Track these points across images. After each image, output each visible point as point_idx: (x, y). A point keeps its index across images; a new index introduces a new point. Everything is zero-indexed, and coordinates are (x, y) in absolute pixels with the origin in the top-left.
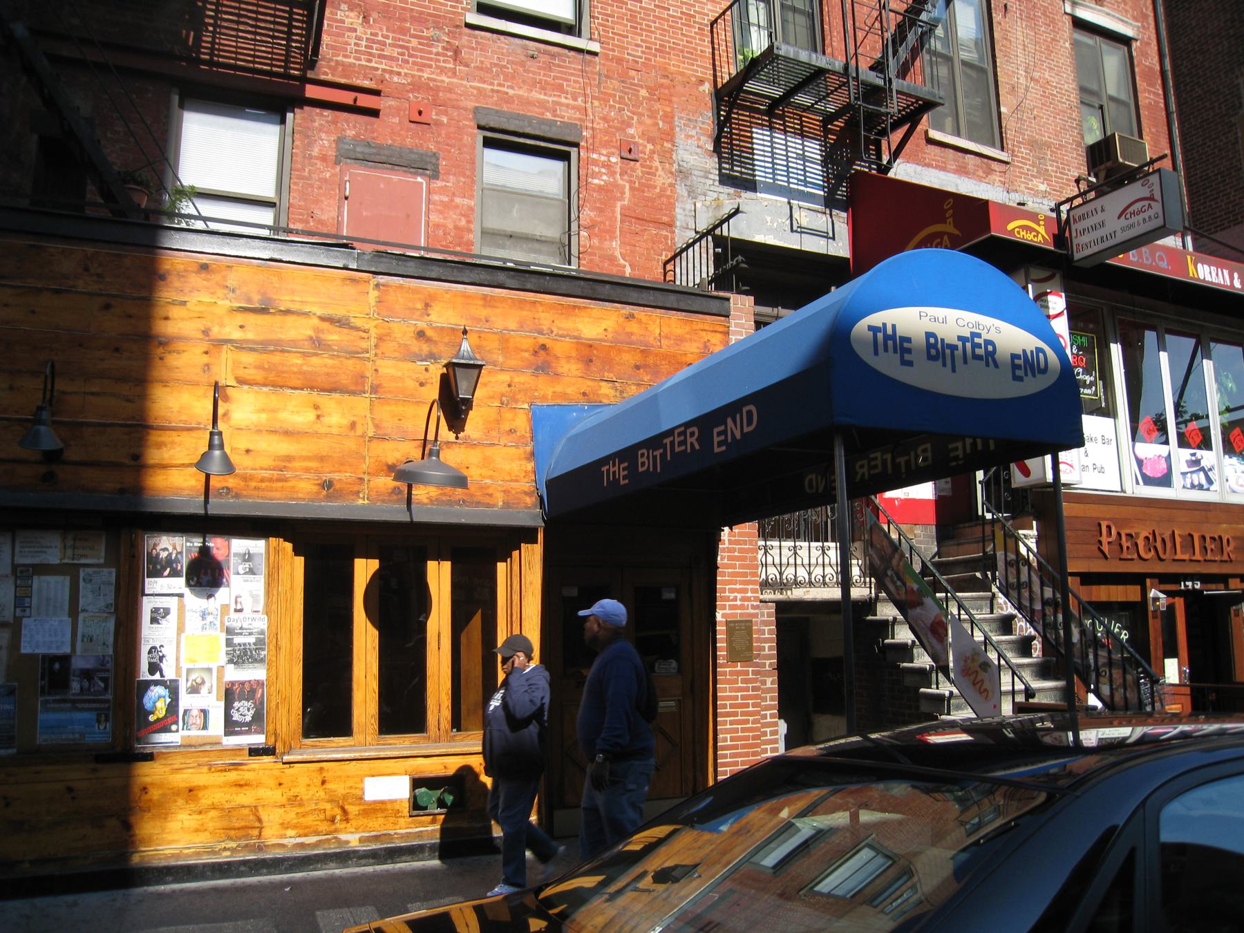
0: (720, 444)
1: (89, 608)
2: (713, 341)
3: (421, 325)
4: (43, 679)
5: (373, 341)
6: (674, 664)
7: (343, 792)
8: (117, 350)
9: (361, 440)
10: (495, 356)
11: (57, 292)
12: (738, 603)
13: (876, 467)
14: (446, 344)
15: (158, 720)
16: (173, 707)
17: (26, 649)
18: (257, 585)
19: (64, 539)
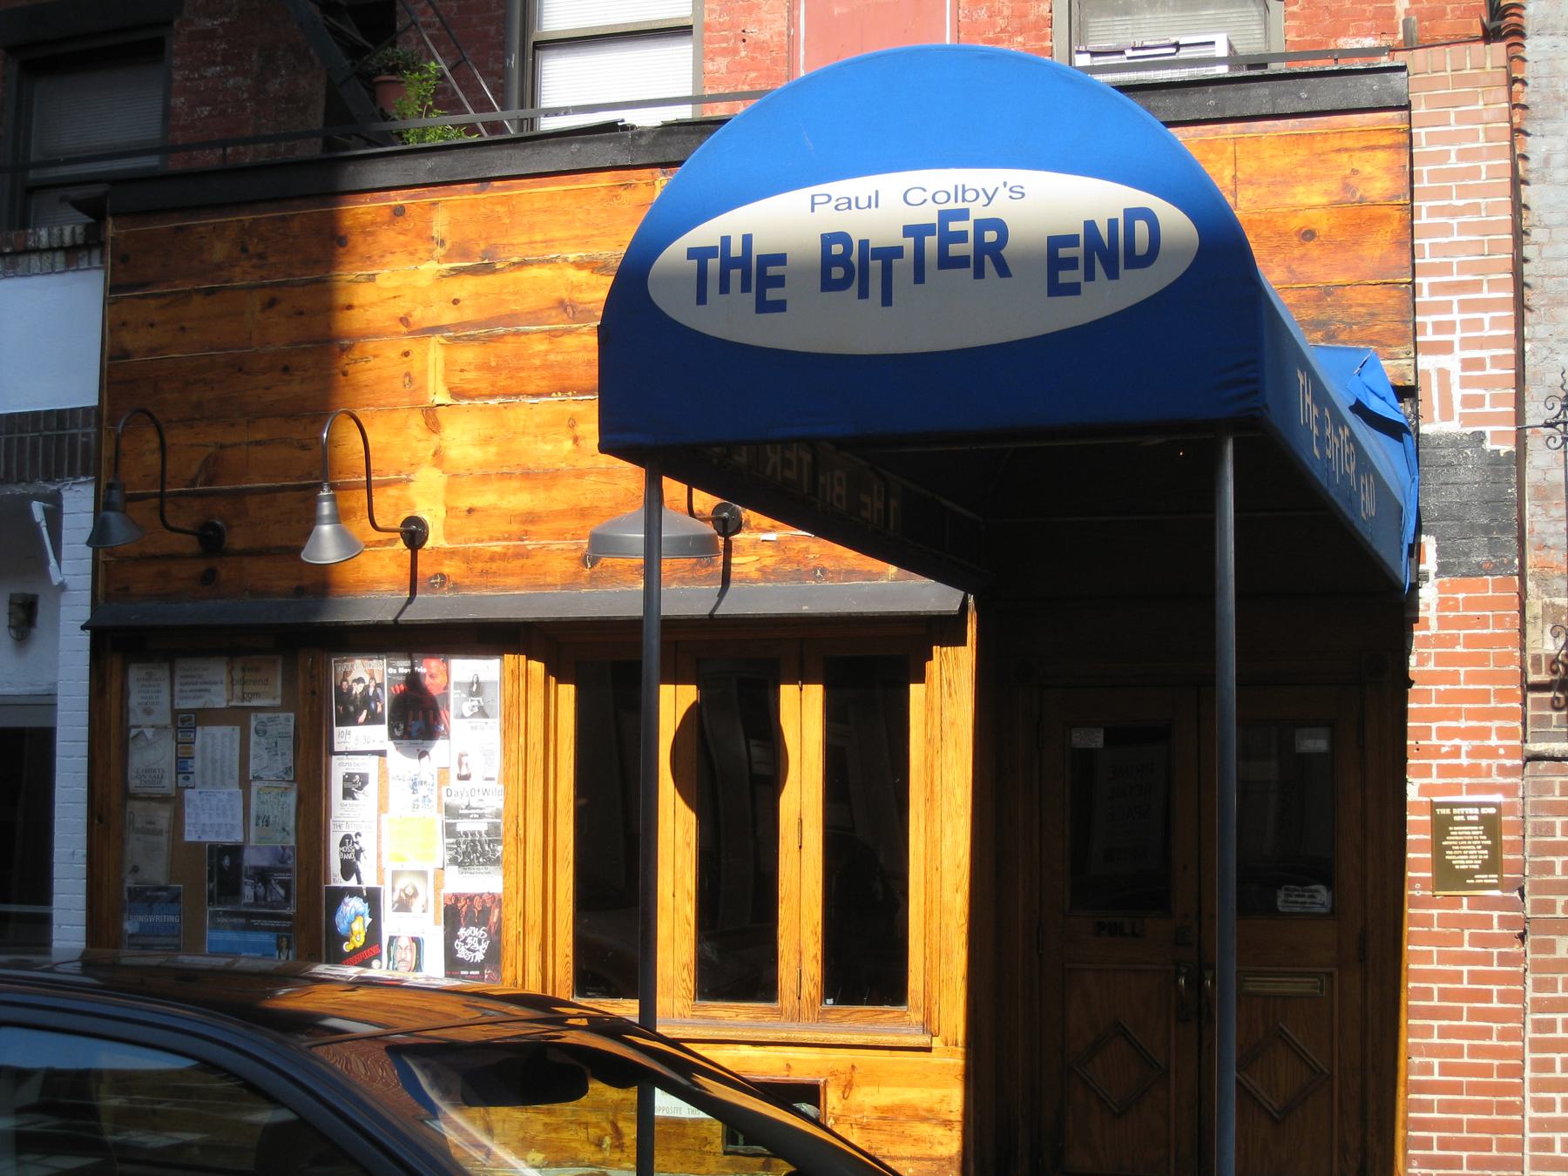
2: (1368, 169)
4: (211, 880)
8: (286, 369)
11: (209, 292)
12: (1464, 761)
15: (355, 951)
16: (374, 932)
17: (190, 836)
18: (491, 730)
19: (231, 671)
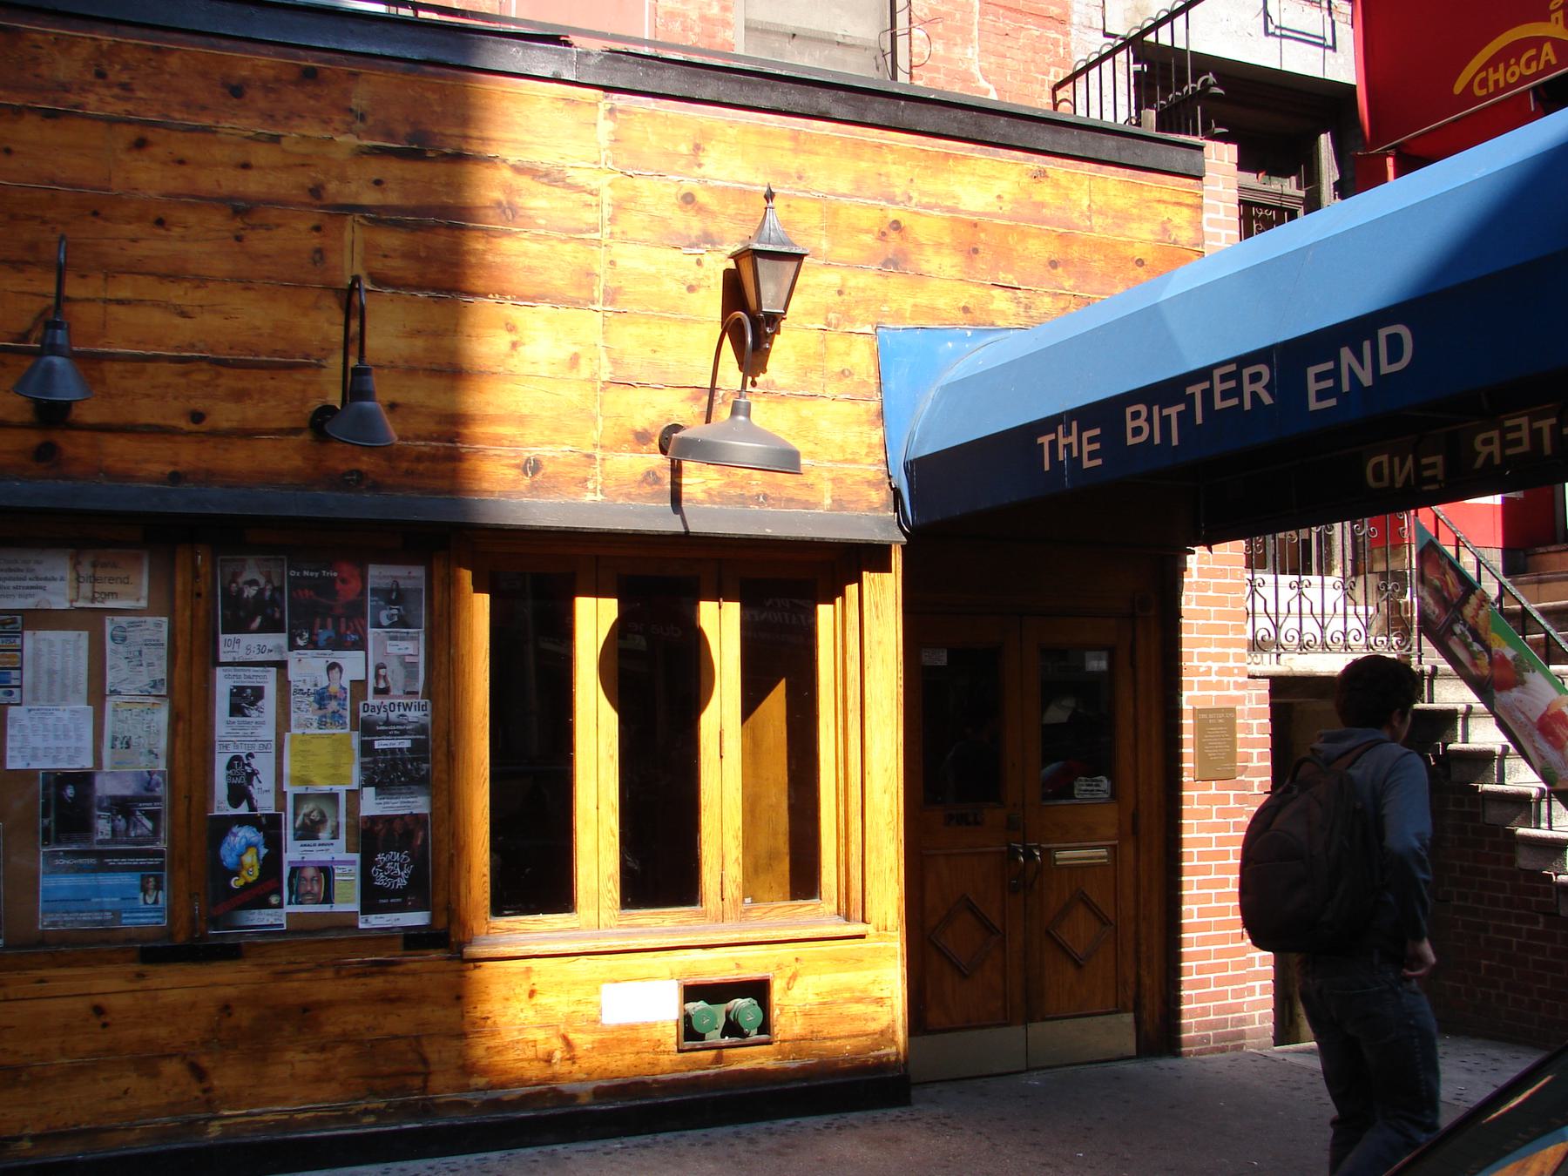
0: (1321, 395)
1: (122, 688)
2: (1177, 221)
3: (689, 185)
5: (607, 211)
6: (1105, 783)
7: (567, 1010)
8: (160, 222)
9: (589, 387)
10: (814, 241)
12: (1214, 678)
13: (1518, 442)
14: (732, 218)
16: (271, 864)
19: (76, 565)
